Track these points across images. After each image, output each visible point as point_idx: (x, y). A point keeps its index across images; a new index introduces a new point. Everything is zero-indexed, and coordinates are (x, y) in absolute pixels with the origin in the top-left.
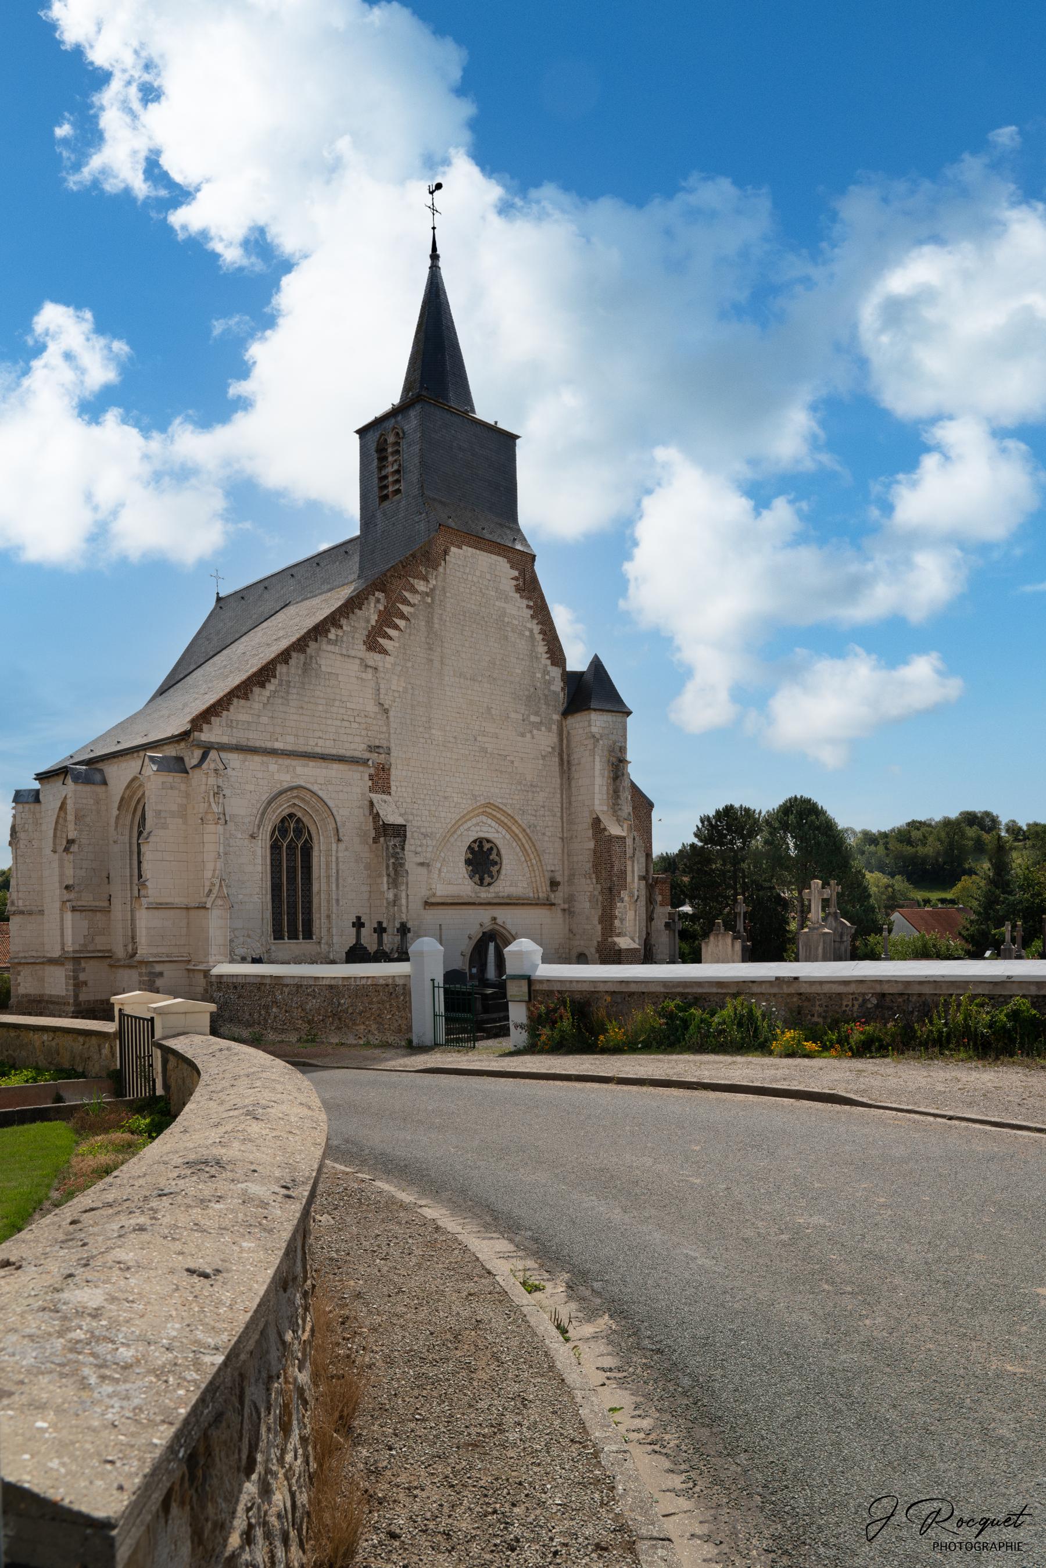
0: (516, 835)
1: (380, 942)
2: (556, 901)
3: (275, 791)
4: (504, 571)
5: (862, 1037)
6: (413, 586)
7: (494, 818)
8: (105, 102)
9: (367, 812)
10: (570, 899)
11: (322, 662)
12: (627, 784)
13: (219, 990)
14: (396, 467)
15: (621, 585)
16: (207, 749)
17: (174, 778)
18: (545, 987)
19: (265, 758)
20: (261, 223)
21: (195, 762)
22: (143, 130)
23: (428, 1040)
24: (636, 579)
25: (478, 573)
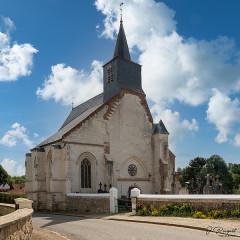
4: (137, 99)
10: (154, 179)
15: (206, 115)
16: (65, 143)
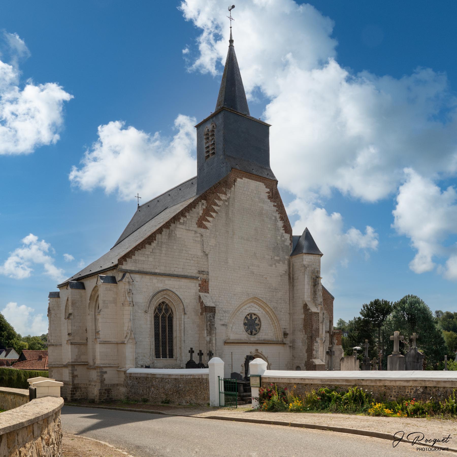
0: (268, 312)
1: (201, 359)
2: (286, 342)
3: (156, 291)
5: (414, 407)
6: (219, 197)
7: (257, 304)
8: (201, 41)
9: (198, 301)
10: (293, 341)
11: (177, 233)
12: (320, 288)
13: (130, 379)
14: (212, 142)
16: (125, 272)
17: (111, 286)
18: (267, 381)
19: (151, 277)
20: (259, 85)
21: (120, 278)
22: (215, 51)
23: (216, 403)
24: (397, 216)
25: (250, 191)
